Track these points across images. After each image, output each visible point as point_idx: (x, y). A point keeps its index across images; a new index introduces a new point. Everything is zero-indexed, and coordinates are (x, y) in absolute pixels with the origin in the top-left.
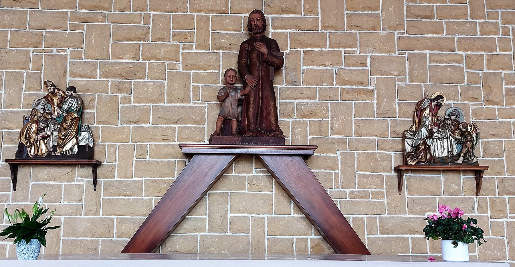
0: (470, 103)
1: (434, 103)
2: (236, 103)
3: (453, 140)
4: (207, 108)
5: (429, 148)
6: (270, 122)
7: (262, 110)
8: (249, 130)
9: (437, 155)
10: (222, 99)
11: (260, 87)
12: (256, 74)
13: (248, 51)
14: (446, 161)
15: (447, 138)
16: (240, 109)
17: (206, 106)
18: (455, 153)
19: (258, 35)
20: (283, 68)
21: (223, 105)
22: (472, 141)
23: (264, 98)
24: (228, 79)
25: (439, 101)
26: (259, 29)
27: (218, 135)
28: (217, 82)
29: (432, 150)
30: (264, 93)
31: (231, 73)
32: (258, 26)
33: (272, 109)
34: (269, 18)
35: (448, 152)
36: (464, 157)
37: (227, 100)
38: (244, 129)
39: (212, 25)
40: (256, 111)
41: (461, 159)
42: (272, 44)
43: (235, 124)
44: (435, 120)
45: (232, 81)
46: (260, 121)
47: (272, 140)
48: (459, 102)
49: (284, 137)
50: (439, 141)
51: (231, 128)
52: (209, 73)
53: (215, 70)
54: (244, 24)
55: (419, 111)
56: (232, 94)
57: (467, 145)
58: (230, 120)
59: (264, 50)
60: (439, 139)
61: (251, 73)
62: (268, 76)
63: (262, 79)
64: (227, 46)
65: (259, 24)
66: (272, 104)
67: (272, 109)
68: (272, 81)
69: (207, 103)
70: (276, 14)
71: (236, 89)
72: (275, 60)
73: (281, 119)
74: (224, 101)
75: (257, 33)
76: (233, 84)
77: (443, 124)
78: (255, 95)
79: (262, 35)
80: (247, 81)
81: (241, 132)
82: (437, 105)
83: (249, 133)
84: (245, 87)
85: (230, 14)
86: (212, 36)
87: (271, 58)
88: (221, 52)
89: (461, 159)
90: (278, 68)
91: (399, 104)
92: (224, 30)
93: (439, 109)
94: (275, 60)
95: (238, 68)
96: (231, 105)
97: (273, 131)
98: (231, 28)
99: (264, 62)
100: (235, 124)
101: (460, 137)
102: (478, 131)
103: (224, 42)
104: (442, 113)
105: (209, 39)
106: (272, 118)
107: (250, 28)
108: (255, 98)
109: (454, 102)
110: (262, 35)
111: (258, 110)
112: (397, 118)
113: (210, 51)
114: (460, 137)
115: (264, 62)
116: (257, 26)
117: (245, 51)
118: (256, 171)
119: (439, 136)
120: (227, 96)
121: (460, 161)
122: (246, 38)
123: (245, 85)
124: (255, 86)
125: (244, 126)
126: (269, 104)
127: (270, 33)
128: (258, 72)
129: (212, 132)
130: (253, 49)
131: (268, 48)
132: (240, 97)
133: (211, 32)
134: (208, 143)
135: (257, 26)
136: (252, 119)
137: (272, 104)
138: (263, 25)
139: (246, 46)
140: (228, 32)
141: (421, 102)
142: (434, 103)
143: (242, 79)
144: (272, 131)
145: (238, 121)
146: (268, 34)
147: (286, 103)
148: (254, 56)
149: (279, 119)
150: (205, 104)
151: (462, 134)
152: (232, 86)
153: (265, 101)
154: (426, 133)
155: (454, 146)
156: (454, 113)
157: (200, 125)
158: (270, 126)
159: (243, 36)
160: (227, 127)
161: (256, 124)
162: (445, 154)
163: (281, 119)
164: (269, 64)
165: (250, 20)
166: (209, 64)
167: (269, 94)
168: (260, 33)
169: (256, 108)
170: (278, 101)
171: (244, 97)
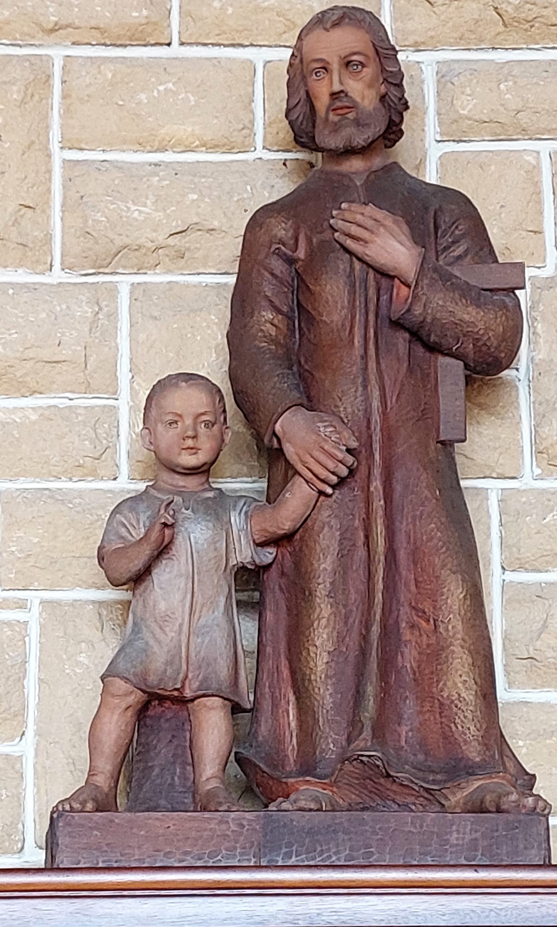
2: (217, 593)
4: (34, 630)
6: (444, 709)
7: (389, 632)
8: (307, 767)
10: (132, 571)
11: (377, 485)
12: (349, 403)
13: (291, 261)
16: (248, 628)
17: (33, 617)
19: (356, 164)
20: (520, 373)
21: (137, 606)
23: (402, 555)
24: (167, 437)
26: (357, 123)
27: (106, 804)
28: (97, 464)
30: (402, 527)
31: (189, 402)
32: (354, 106)
33: (454, 624)
34: (422, 67)
37: (162, 574)
38: (276, 760)
39: (67, 112)
40: (353, 641)
42: (445, 221)
43: (213, 730)
45: (194, 450)
46: (382, 704)
47: (464, 830)
49: (541, 812)
51: (189, 755)
52: (50, 415)
53: (88, 388)
54: (266, 106)
56: (195, 534)
58: (182, 701)
59: (394, 248)
61: (310, 402)
62: (426, 414)
63: (388, 440)
64: (161, 239)
65: (362, 91)
66: (454, 594)
67: (454, 624)
68: (447, 445)
69: (34, 598)
70: (463, 42)
71: (218, 506)
72: (469, 314)
73: (518, 695)
74: (139, 579)
75: (350, 152)
76: (203, 471)
78: (345, 537)
79: (377, 162)
80: (289, 450)
81: (256, 780)
83: (307, 792)
84: (273, 496)
85: (176, 50)
86: (68, 181)
87: (440, 307)
88: (124, 282)
90: (487, 365)
92: (141, 145)
94: (469, 314)
95: (233, 378)
96: (193, 618)
97: (471, 770)
98: (185, 130)
99: (397, 324)
100: (213, 730)
103: (146, 217)
105: (47, 203)
106: (459, 683)
107: (303, 126)
108: (344, 556)
110: (377, 162)
111: (365, 638)
113: (57, 276)
115: (397, 324)
116: (346, 123)
117: (278, 266)
118: (149, 684)
120: (163, 550)
122: (281, 188)
123: (273, 460)
124: (342, 481)
125: (278, 739)
126: (434, 597)
127: (430, 155)
128: (362, 385)
129: (67, 782)
130: (329, 248)
131: (418, 238)
132: (244, 554)
133: (58, 156)
134: (37, 857)
135: (346, 123)
136: (326, 696)
137: (454, 594)
138: (383, 98)
139: (281, 229)
140: (168, 157)
143: (258, 437)
144: (459, 769)
145: (236, 709)
146: (421, 165)
147: (541, 593)
148: (334, 294)
149: (503, 693)
150: (22, 605)
152: (192, 483)
153: (406, 572)
158: (448, 738)
159: (265, 171)
160: (163, 752)
161: (354, 725)
163: (518, 695)
164: (425, 340)
165: (301, 71)
166: (46, 354)
167: (433, 530)
168: (363, 151)
169: (356, 618)
170: (495, 580)
171: (268, 555)
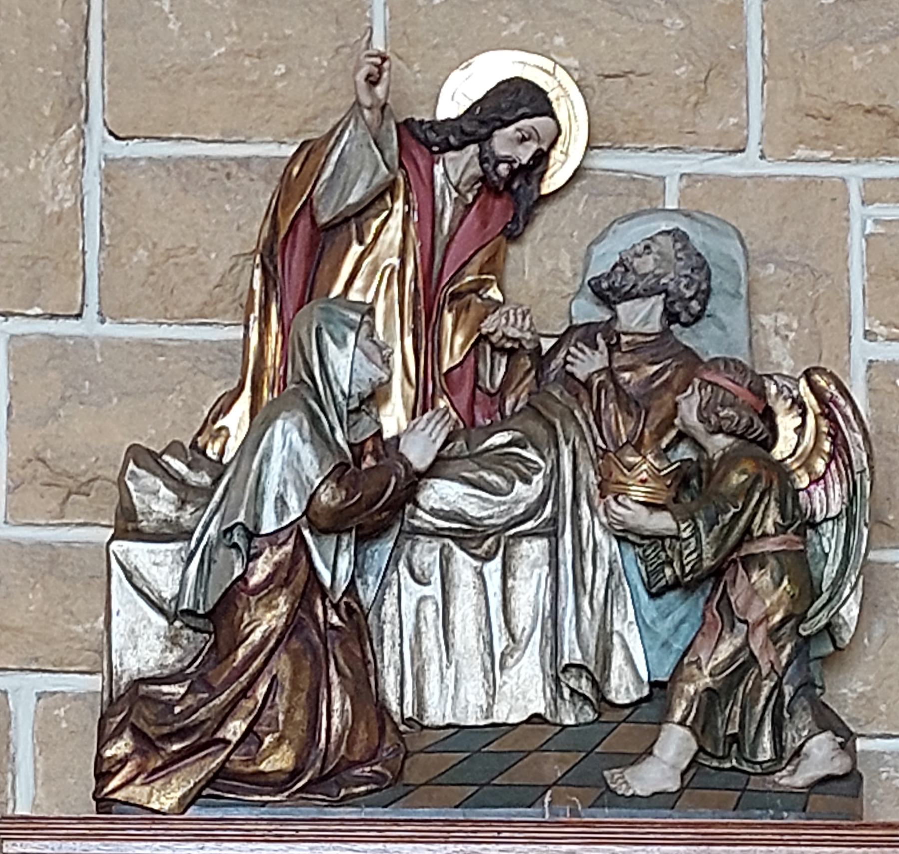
0: (856, 173)
1: (455, 168)
3: (608, 547)
5: (359, 625)
9: (435, 715)
14: (520, 774)
15: (551, 532)
18: (623, 688)
22: (799, 568)
25: (503, 142)
29: (389, 655)
35: (557, 673)
36: (702, 724)
41: (675, 745)
44: (454, 346)
48: (746, 165)
50: (463, 564)
55: (301, 246)
57: (738, 597)
60: (469, 535)
77: (508, 394)
82: (488, 186)
89: (675, 745)
91: (113, 171)
93: (513, 235)
101: (663, 522)
102: (859, 456)
104: (543, 280)
109: (693, 164)
112: (89, 326)
114: (663, 522)
119: (473, 510)
121: (658, 773)
141: (311, 152)
142: (455, 168)
151: (689, 486)
153: (442, 641)
154: (312, 468)
155: (625, 625)
156: (647, 264)
157: (739, 274)
162: (524, 692)
